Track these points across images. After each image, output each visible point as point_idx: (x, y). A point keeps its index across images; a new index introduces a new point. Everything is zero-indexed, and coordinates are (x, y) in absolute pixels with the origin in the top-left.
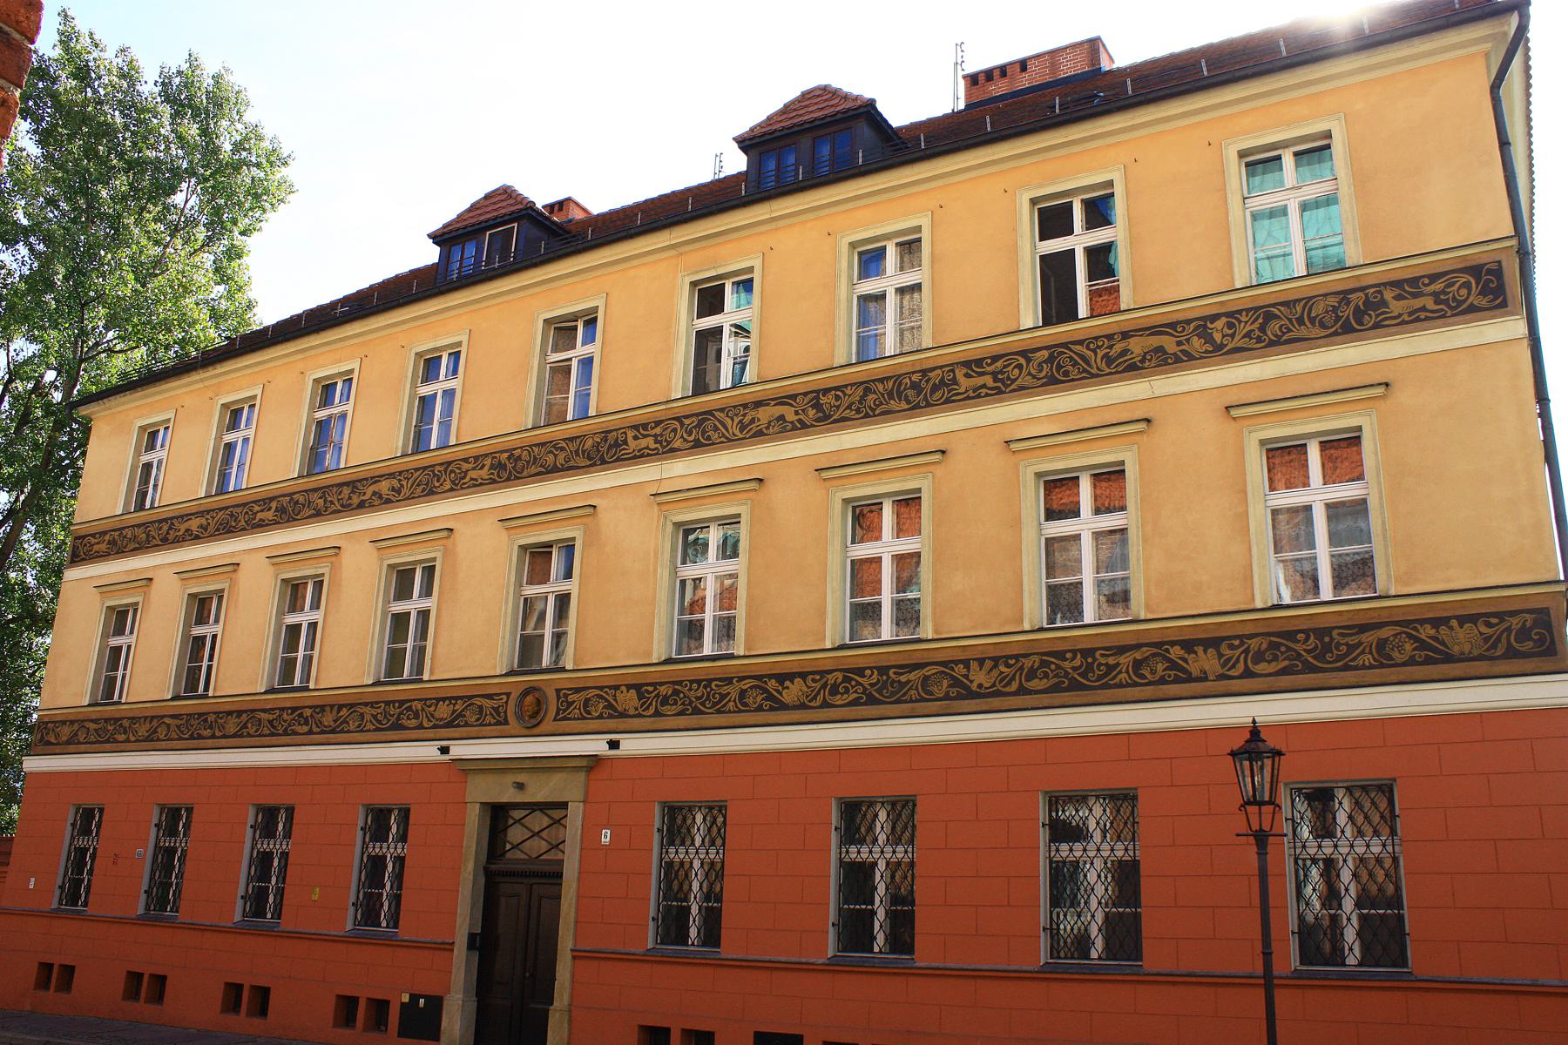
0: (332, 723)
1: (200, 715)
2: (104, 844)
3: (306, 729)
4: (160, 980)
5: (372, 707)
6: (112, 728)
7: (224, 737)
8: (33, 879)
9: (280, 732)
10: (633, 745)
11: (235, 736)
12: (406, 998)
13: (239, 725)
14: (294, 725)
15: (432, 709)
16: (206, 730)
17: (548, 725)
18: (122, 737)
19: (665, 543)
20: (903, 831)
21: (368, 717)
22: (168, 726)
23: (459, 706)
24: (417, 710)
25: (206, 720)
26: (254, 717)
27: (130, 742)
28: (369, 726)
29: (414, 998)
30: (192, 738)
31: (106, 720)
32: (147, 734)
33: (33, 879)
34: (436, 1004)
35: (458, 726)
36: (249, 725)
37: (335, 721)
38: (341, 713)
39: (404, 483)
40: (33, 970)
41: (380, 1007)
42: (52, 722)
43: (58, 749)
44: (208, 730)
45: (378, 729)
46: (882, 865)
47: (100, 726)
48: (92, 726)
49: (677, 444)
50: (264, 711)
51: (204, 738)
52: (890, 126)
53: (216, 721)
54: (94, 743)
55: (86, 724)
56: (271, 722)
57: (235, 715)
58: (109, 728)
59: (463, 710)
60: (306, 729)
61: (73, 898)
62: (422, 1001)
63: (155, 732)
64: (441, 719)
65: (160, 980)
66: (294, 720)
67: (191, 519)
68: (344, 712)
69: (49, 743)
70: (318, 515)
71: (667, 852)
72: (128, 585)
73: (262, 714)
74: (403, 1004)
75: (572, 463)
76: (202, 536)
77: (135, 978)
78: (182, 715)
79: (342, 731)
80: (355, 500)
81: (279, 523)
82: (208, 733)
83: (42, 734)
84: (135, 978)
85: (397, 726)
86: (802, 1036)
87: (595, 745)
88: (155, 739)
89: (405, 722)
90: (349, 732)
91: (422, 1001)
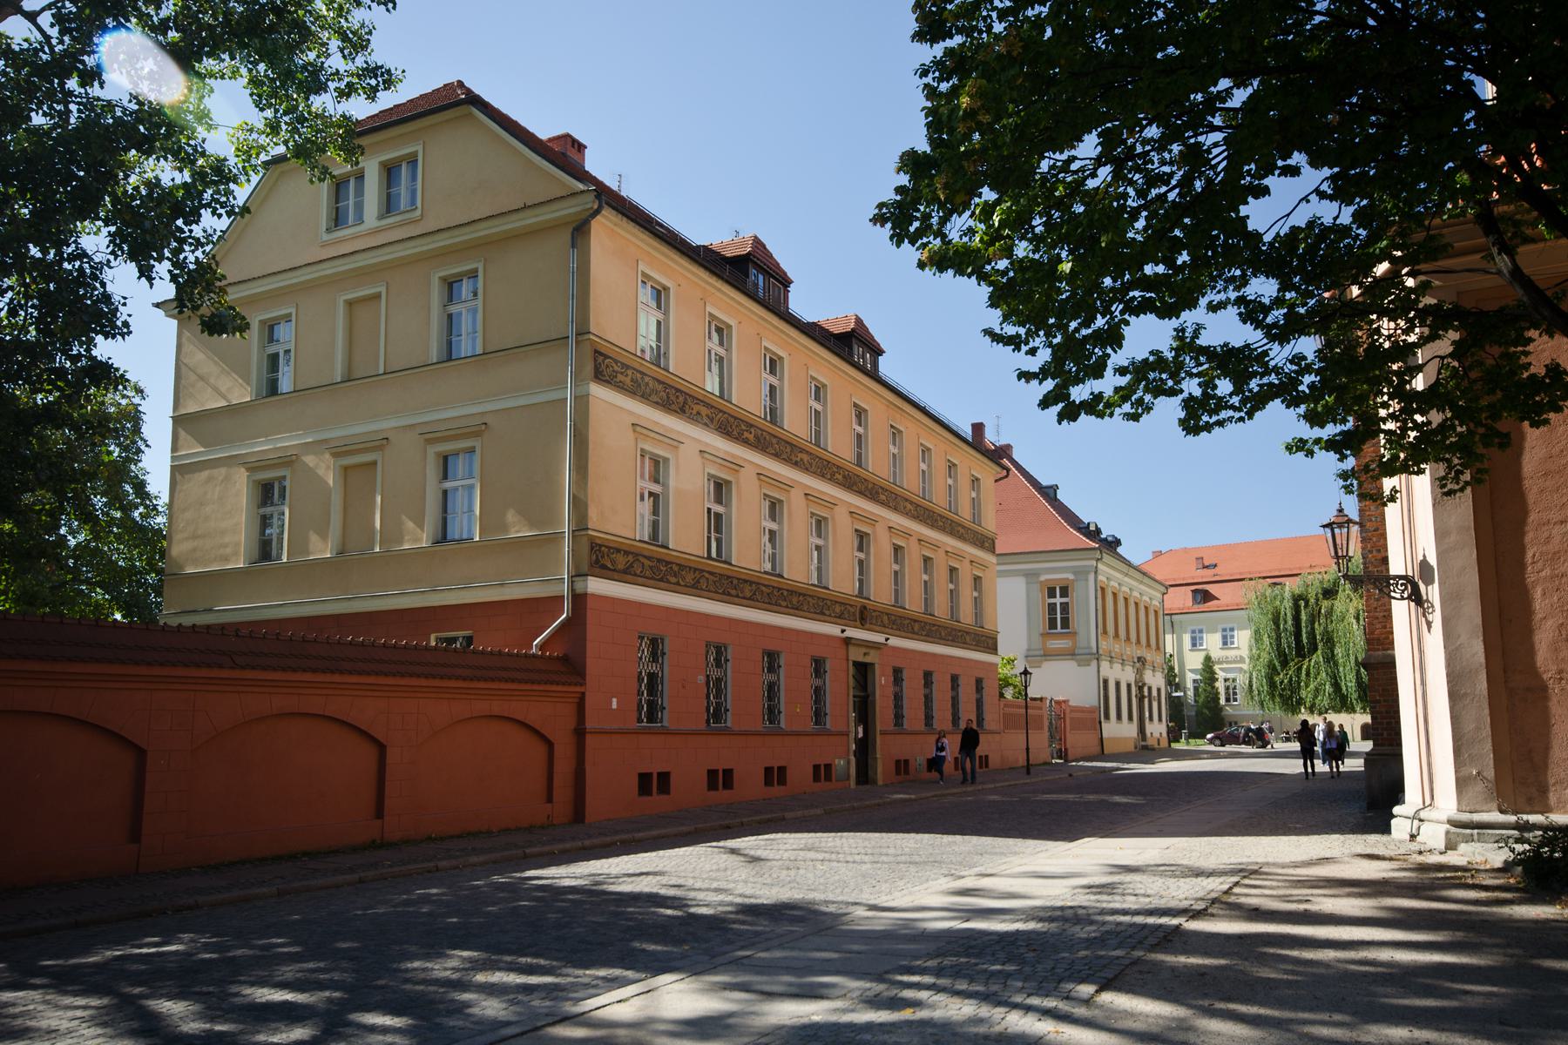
1: (729, 577)
2: (668, 671)
7: (744, 598)
8: (614, 700)
10: (895, 642)
11: (749, 599)
17: (867, 626)
18: (673, 580)
19: (704, 488)
22: (707, 579)
23: (630, 558)
25: (732, 582)
27: (680, 585)
30: (723, 593)
31: (659, 560)
33: (614, 700)
40: (810, 770)
42: (606, 547)
43: (616, 575)
47: (653, 564)
48: (647, 562)
50: (765, 586)
51: (732, 596)
52: (541, 140)
54: (651, 579)
55: (641, 559)
61: (652, 717)
65: (782, 770)
68: (801, 598)
69: (604, 567)
70: (777, 456)
72: (774, 482)
77: (712, 774)
83: (597, 556)
84: (712, 774)
85: (823, 613)
87: (878, 638)
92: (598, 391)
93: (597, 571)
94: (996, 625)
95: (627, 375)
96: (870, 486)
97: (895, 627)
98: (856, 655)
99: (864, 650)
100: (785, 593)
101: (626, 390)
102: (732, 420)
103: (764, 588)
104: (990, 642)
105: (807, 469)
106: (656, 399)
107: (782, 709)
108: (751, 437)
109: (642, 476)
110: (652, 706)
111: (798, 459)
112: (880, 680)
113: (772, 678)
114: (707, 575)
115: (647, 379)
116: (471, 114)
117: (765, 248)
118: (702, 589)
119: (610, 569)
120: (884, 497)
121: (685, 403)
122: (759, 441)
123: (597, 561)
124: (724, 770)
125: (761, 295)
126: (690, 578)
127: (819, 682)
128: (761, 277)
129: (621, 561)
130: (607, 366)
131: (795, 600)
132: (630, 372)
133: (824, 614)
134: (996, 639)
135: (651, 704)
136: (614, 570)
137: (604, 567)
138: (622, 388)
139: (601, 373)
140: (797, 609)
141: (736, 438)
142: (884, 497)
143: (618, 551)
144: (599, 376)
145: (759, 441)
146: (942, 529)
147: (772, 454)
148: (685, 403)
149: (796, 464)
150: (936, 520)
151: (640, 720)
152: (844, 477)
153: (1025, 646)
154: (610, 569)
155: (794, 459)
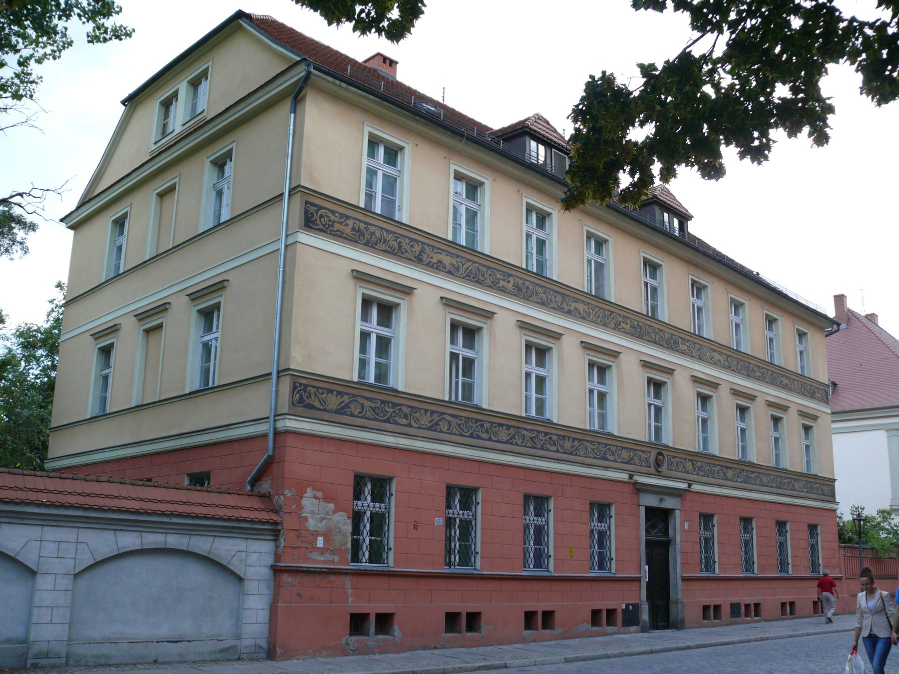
0: (570, 449)
3: (555, 448)
4: (757, 606)
5: (591, 443)
6: (392, 410)
9: (539, 447)
12: (624, 607)
13: (508, 435)
14: (395, 416)
15: (620, 452)
16: (484, 433)
20: (378, 497)
21: (589, 449)
22: (449, 422)
23: (346, 399)
24: (407, 414)
25: (482, 426)
26: (636, 454)
28: (590, 455)
29: (627, 606)
30: (471, 436)
32: (429, 425)
34: (637, 607)
35: (631, 464)
36: (517, 437)
37: (430, 422)
38: (575, 443)
39: (591, 311)
41: (611, 613)
44: (485, 434)
45: (595, 458)
46: (368, 514)
49: (694, 354)
53: (491, 429)
54: (372, 419)
55: (359, 399)
56: (532, 439)
57: (505, 427)
58: (387, 409)
59: (438, 421)
60: (555, 448)
62: (631, 607)
63: (437, 424)
64: (624, 459)
65: (757, 606)
66: (547, 440)
67: (442, 254)
68: (576, 443)
69: (310, 407)
71: (473, 516)
73: (525, 432)
74: (623, 610)
75: (661, 343)
76: (455, 274)
78: (376, 399)
79: (576, 455)
80: (566, 308)
81: (517, 296)
82: (485, 435)
83: (301, 396)
86: (446, 613)
88: (514, 443)
89: (608, 456)
90: (580, 456)
91: (631, 607)
92: (306, 238)
93: (300, 410)
94: (833, 474)
95: (509, 282)
96: (809, 387)
97: (702, 473)
98: (652, 501)
99: (659, 497)
100: (555, 438)
101: (345, 238)
102: (485, 269)
103: (525, 432)
104: (826, 489)
105: (583, 318)
106: (383, 247)
107: (716, 559)
108: (510, 286)
109: (737, 420)
110: (602, 557)
111: (572, 308)
112: (682, 525)
113: (747, 536)
114: (449, 418)
115: (372, 229)
116: (241, 27)
117: (548, 123)
118: (441, 431)
119: (318, 409)
120: (685, 347)
121: (422, 251)
122: (520, 289)
123: (301, 400)
124: (543, 612)
125: (677, 233)
126: (425, 420)
127: (707, 534)
128: (666, 215)
129: (333, 401)
130: (321, 216)
131: (568, 445)
132: (511, 280)
133: (606, 459)
134: (833, 487)
135: (601, 555)
136: (325, 410)
137: (310, 407)
138: (340, 236)
139: (314, 222)
140: (570, 454)
141: (490, 287)
142: (820, 395)
143: (330, 391)
144: (309, 223)
145: (520, 289)
146: (762, 379)
147: (538, 303)
148: (422, 251)
149: (569, 312)
150: (753, 371)
151: (355, 558)
152: (633, 327)
153: (890, 497)
154: (318, 409)
155: (566, 308)
